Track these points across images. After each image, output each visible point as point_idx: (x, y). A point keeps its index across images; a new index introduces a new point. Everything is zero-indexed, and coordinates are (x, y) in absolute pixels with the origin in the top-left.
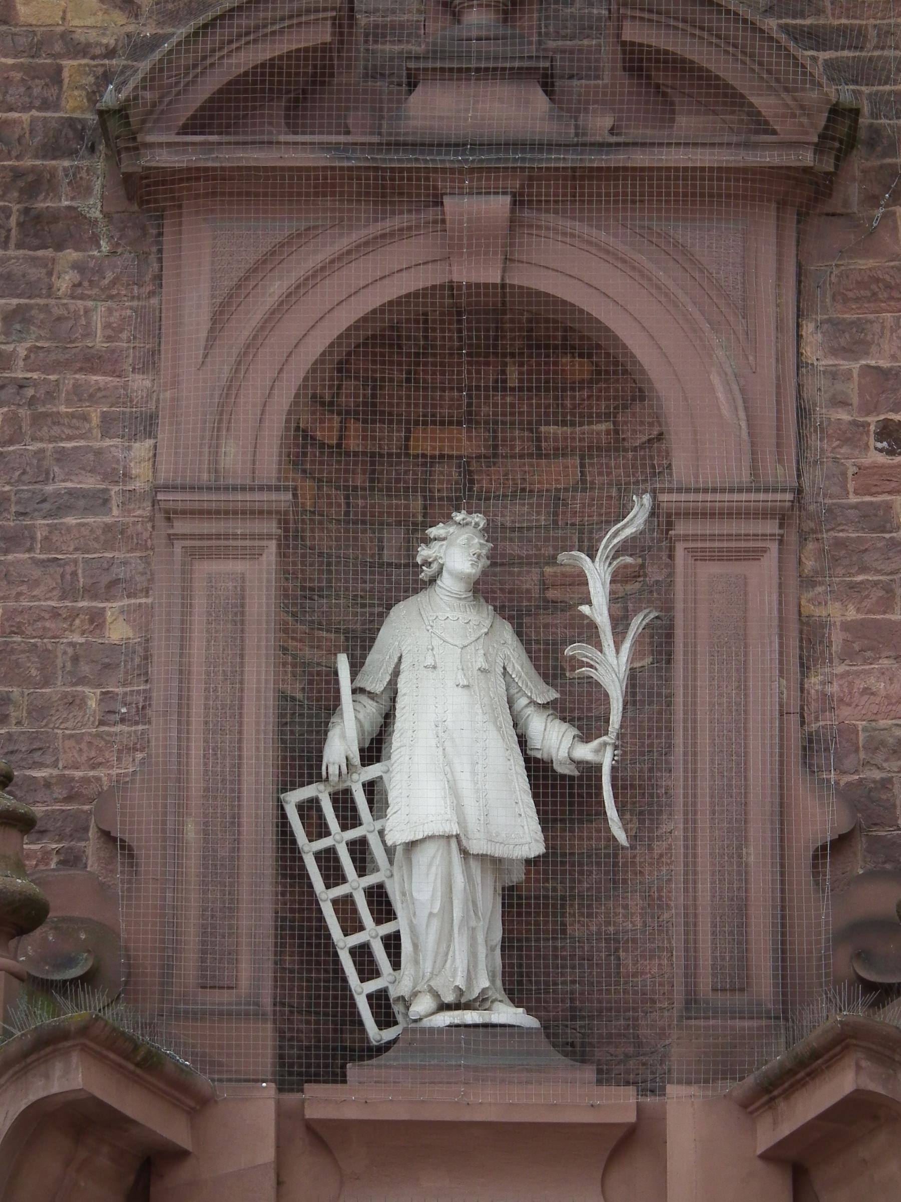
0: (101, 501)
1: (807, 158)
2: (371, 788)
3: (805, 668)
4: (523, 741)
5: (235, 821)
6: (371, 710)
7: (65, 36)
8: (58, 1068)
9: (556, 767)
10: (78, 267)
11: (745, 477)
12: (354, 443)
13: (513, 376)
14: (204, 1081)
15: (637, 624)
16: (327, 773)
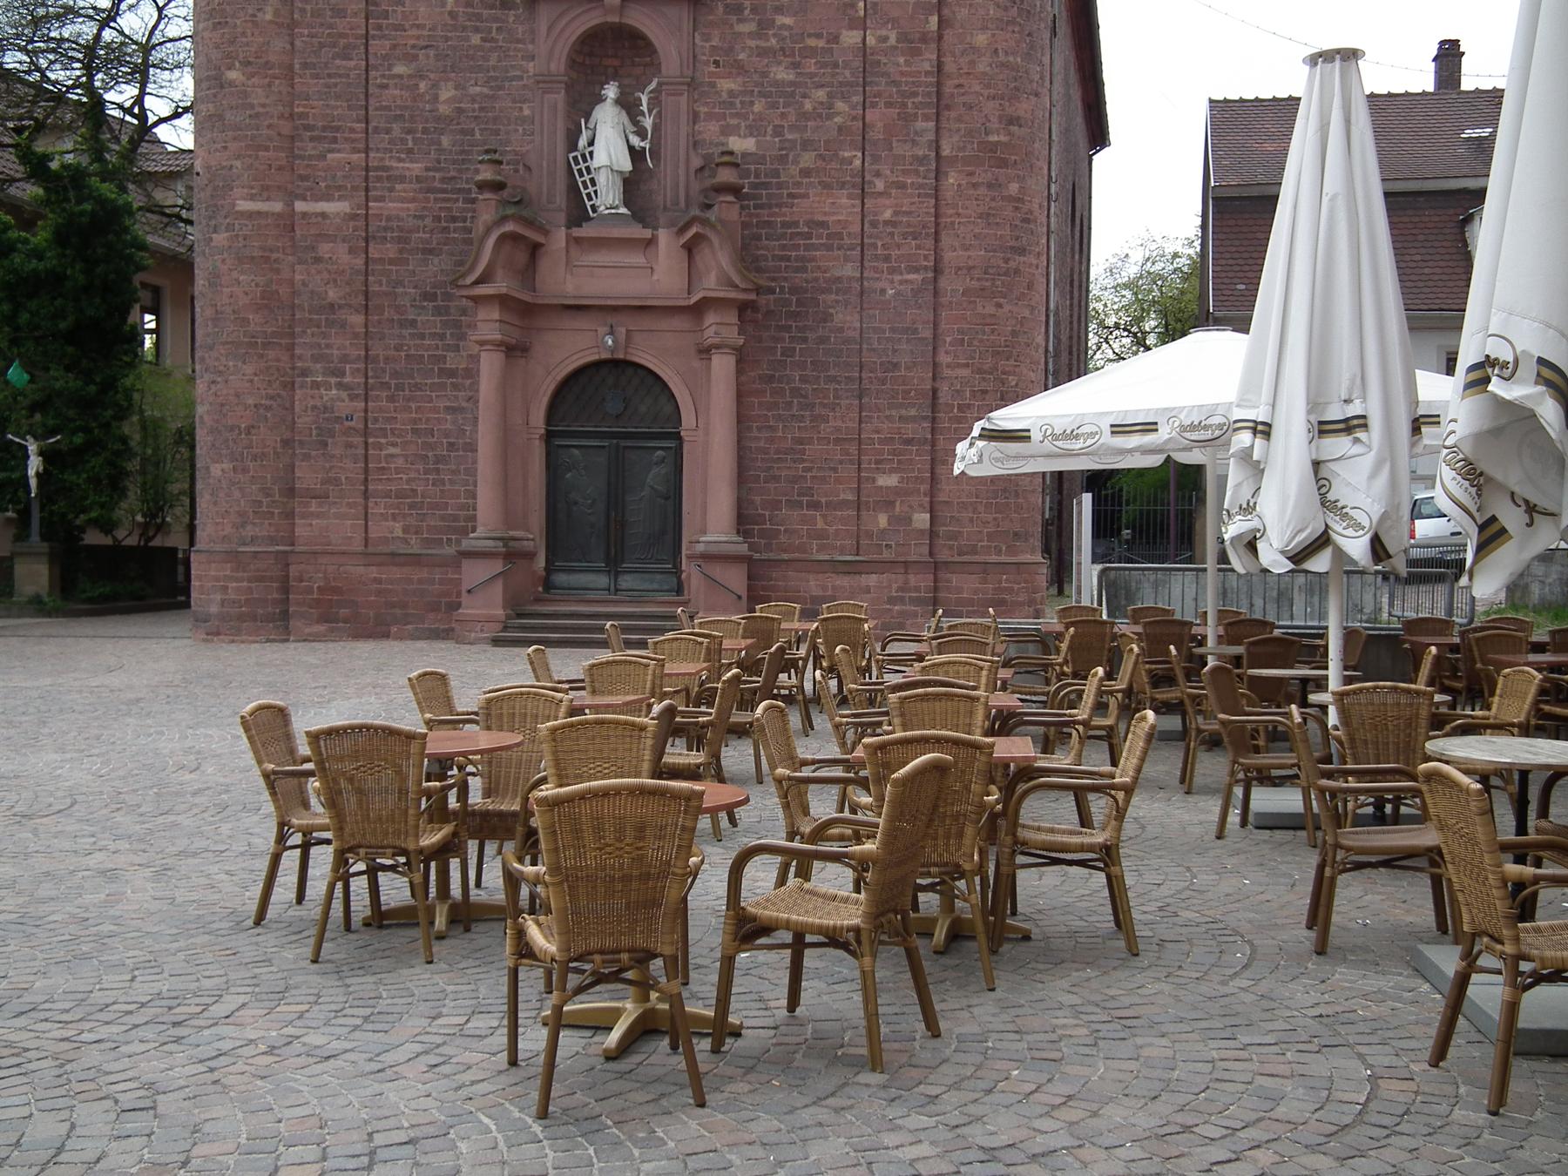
0: (521, 78)
3: (694, 123)
4: (628, 141)
6: (590, 132)
9: (130, 428)
11: (678, 73)
12: (587, 62)
13: (627, 44)
14: (547, 227)
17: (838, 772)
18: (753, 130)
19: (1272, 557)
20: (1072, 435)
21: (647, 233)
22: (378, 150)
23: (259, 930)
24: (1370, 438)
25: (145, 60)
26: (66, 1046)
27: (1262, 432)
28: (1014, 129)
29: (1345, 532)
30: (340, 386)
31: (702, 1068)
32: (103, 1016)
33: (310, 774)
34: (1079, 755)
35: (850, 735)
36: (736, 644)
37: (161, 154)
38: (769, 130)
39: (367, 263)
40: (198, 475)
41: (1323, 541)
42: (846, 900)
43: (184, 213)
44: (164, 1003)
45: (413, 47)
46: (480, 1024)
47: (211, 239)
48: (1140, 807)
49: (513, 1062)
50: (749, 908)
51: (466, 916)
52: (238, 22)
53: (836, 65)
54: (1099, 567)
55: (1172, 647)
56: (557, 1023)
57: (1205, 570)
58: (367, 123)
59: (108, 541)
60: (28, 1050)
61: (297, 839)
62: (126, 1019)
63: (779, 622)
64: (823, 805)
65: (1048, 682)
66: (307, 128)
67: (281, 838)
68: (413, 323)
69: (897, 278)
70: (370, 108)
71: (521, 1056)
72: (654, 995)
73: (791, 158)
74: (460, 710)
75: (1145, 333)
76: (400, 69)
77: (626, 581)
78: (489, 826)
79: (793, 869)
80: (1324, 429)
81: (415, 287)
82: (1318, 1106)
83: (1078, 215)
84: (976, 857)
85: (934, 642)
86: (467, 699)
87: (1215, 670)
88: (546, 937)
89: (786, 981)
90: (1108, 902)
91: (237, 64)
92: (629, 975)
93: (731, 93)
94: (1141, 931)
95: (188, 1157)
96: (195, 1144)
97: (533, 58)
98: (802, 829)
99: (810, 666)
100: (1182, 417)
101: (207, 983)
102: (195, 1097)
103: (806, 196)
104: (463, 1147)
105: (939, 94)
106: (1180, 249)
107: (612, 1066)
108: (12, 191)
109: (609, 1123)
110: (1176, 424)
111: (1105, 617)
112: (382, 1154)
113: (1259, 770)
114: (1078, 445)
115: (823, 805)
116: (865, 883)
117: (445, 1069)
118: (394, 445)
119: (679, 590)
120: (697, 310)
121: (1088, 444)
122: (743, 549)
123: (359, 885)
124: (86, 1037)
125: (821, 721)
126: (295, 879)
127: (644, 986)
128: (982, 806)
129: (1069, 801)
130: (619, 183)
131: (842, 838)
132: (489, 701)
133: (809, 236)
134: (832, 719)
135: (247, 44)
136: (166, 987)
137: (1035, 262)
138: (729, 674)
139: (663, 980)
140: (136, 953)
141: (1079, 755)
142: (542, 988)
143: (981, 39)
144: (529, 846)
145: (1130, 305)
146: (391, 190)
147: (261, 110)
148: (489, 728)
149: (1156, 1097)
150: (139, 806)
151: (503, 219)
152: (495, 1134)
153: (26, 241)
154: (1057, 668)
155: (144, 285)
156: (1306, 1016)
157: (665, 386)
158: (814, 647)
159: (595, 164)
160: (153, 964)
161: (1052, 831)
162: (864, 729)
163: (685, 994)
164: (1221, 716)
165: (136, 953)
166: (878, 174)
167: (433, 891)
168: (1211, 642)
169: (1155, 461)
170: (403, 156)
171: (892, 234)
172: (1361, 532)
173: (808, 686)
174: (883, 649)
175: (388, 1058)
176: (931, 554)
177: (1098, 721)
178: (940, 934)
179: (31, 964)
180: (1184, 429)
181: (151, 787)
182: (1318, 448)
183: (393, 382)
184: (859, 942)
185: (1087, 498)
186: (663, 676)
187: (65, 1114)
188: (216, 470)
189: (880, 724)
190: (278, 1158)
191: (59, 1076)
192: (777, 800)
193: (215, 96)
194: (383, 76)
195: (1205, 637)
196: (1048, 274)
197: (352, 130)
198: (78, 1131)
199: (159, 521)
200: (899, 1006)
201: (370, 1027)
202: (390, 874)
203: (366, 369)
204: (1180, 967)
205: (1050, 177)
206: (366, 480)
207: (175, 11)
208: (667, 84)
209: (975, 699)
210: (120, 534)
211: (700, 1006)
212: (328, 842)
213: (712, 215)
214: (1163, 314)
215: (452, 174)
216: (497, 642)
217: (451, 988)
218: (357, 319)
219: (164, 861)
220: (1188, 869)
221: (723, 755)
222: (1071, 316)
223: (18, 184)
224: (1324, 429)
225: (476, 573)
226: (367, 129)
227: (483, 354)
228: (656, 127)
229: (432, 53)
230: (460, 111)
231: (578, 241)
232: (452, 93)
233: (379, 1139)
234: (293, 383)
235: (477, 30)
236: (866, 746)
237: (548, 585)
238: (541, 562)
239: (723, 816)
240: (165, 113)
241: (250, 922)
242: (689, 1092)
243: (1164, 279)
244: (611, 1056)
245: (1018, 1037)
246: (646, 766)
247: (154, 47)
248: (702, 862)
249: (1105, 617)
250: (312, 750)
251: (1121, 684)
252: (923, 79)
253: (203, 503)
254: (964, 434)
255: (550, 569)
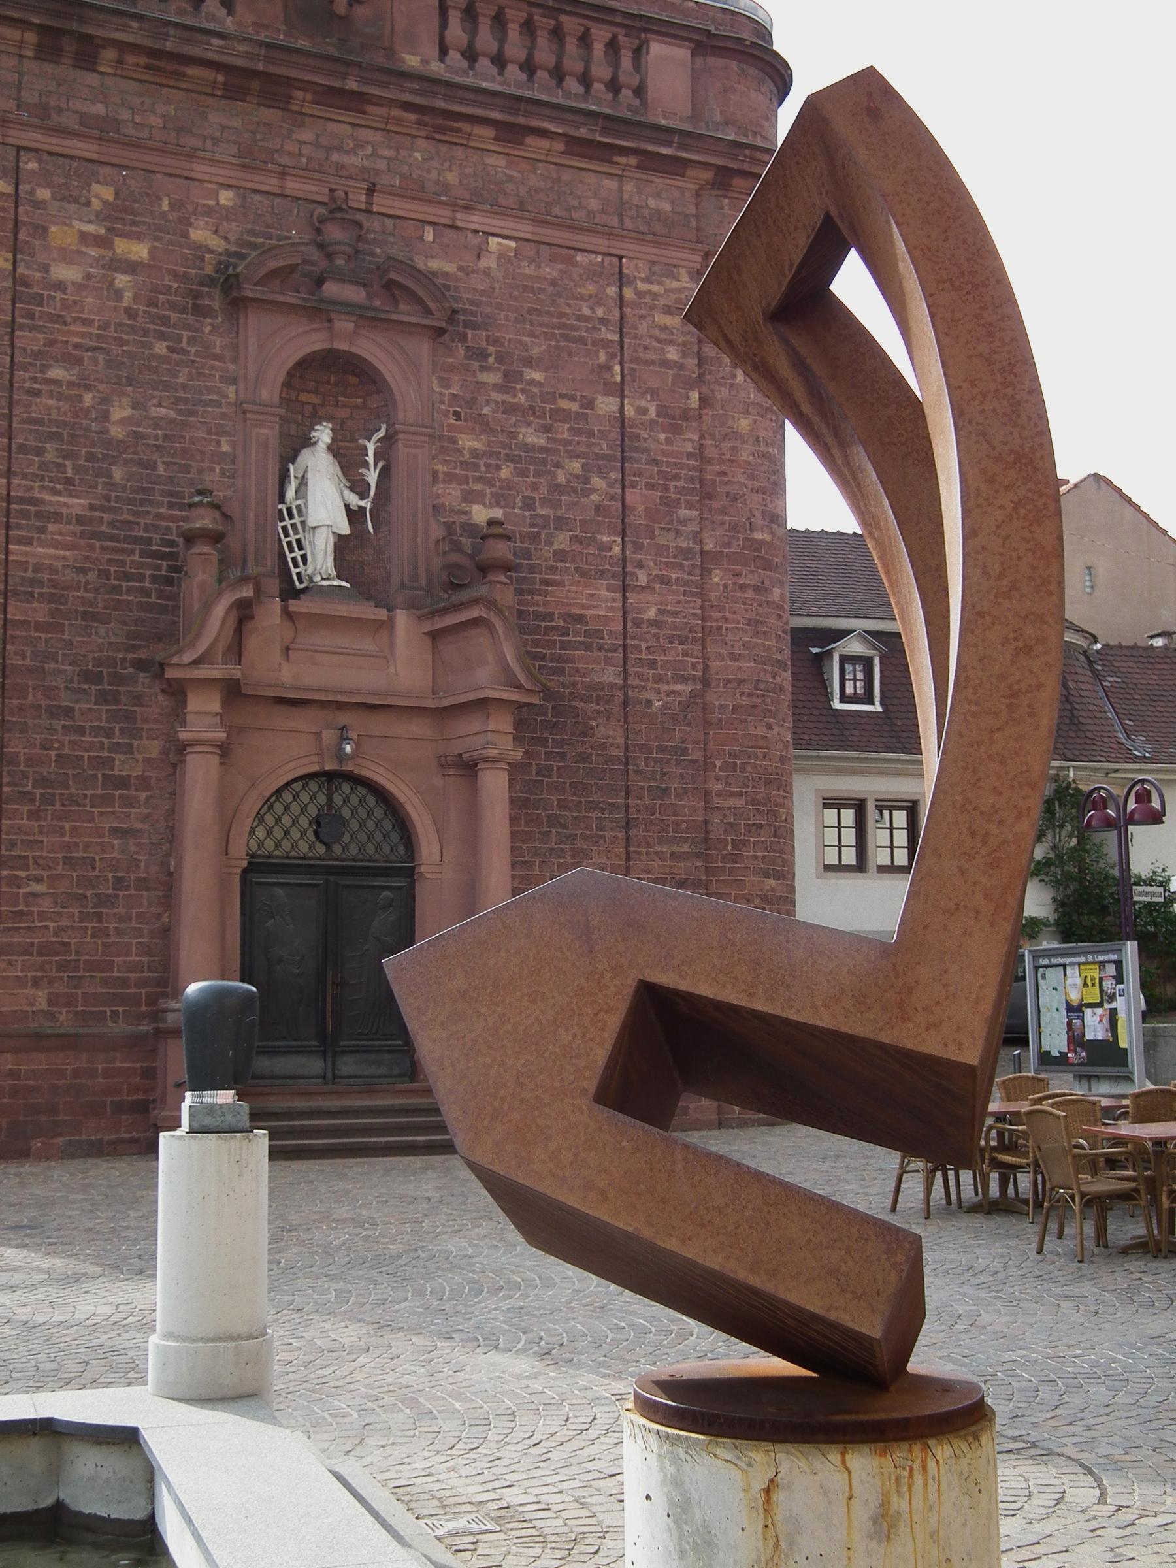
0: (218, 404)
2: (298, 507)
5: (266, 514)
7: (206, 246)
8: (245, 588)
10: (211, 325)
13: (333, 379)
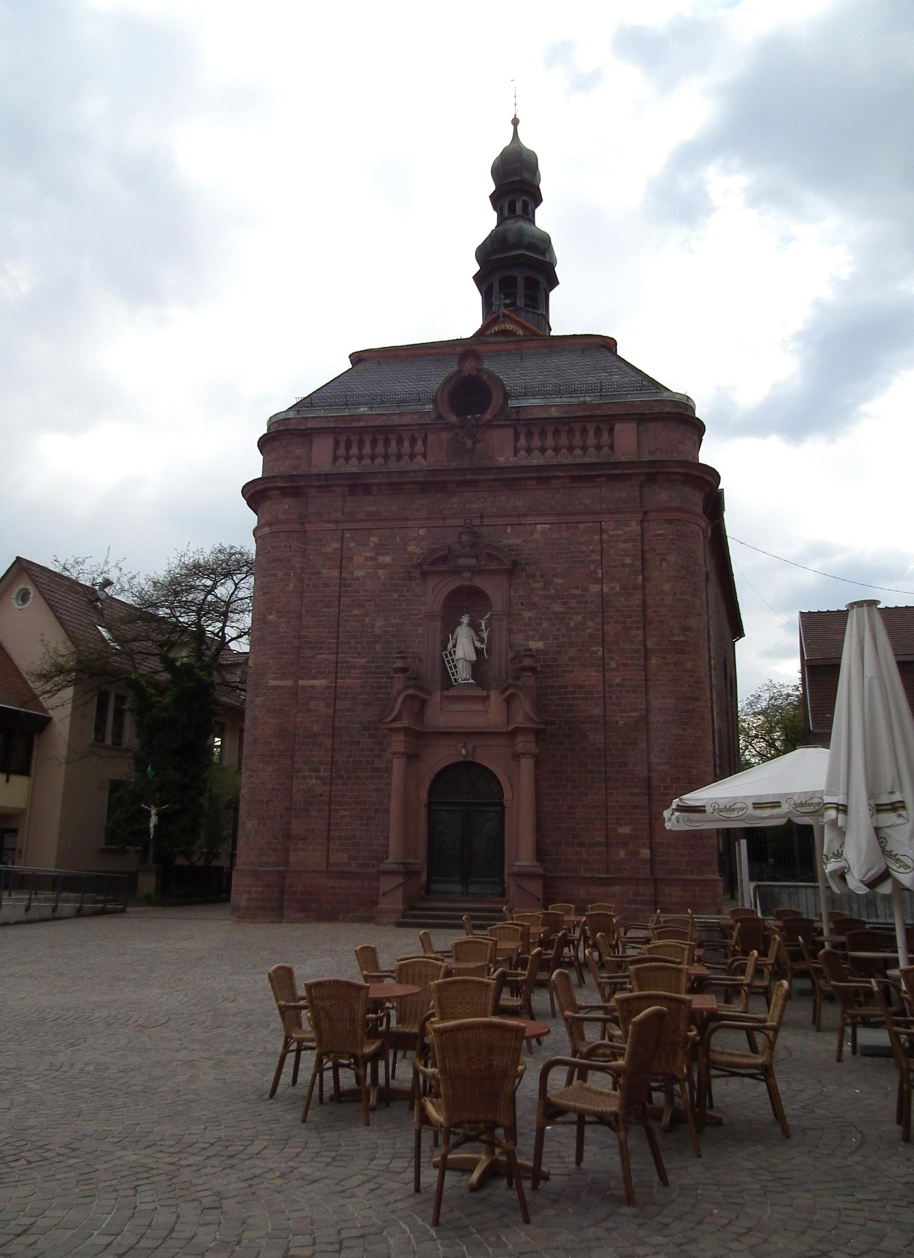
0: (418, 614)
1: (510, 567)
3: (510, 634)
4: (474, 645)
9: (204, 800)
15: (489, 629)
16: (394, 863)
17: (600, 1014)
18: (541, 638)
19: (855, 883)
20: (730, 809)
21: (485, 693)
22: (343, 653)
23: (272, 1101)
24: (908, 814)
25: (227, 609)
26: (172, 1167)
27: (842, 810)
28: (687, 633)
29: (899, 870)
30: (318, 778)
31: (527, 1198)
32: (191, 1150)
33: (305, 1007)
34: (747, 1005)
35: (607, 990)
36: (538, 930)
37: (230, 654)
38: (551, 637)
39: (334, 712)
40: (240, 827)
41: (885, 875)
42: (608, 1095)
43: (240, 686)
44: (224, 1143)
45: (363, 601)
46: (397, 1165)
47: (254, 700)
48: (785, 1039)
49: (417, 1189)
50: (552, 1098)
51: (388, 1096)
52: (275, 592)
53: (587, 603)
54: (753, 884)
55: (800, 937)
56: (444, 1166)
57: (818, 887)
58: (338, 639)
59: (188, 863)
60: (152, 1169)
61: (294, 1046)
62: (203, 1152)
63: (562, 916)
64: (592, 1034)
65: (727, 957)
66: (307, 643)
67: (286, 1045)
68: (358, 743)
69: (625, 715)
70: (340, 632)
71: (422, 1186)
72: (498, 1151)
73: (563, 652)
74: (382, 969)
75: (774, 740)
76: (355, 612)
77: (473, 889)
78: (401, 1042)
79: (576, 1073)
80: (879, 809)
81: (360, 723)
82: (907, 1243)
83: (728, 675)
84: (685, 1070)
85: (656, 932)
86: (387, 962)
87: (827, 954)
88: (437, 1112)
89: (574, 1145)
90: (769, 1101)
91: (274, 612)
92: (483, 1137)
93: (530, 618)
94: (791, 1122)
95: (240, 1238)
96: (243, 1231)
97: (424, 604)
98: (580, 1049)
99: (582, 943)
100: (795, 798)
101: (246, 1133)
102: (242, 1202)
103: (572, 671)
104: (391, 1241)
105: (645, 616)
106: (791, 692)
107: (474, 1195)
108: (157, 677)
109: (474, 1231)
110: (792, 803)
111: (759, 915)
112: (346, 1243)
113: (863, 1017)
114: (735, 814)
115: (592, 1034)
116: (619, 1085)
117: (379, 1192)
118: (345, 810)
119: (503, 894)
120: (513, 734)
121: (740, 814)
122: (540, 870)
123: (328, 1075)
124: (183, 1162)
125: (589, 978)
126: (292, 1071)
127: (492, 1145)
128: (687, 1038)
129: (743, 1035)
130: (469, 667)
131: (604, 1055)
132: (401, 966)
133: (573, 693)
134: (596, 979)
135: (279, 602)
136: (223, 1135)
137: (704, 705)
138: (535, 951)
139: (504, 1141)
140: (207, 1112)
141: (747, 1005)
142: (432, 1144)
143: (667, 587)
144: (425, 1053)
145: (764, 723)
146: (349, 673)
147: (284, 634)
148: (400, 982)
149: (804, 1232)
150: (204, 1022)
151: (407, 688)
152: (409, 1234)
153: (160, 702)
154: (731, 948)
155: (217, 723)
156: (898, 1182)
157: (494, 776)
158: (583, 932)
159: (457, 657)
160: (215, 1120)
161: (731, 1054)
162: (616, 987)
163: (516, 1151)
164: (833, 983)
165: (207, 1112)
166: (612, 659)
167: (368, 1080)
168: (826, 933)
169: (781, 822)
170: (356, 655)
171: (621, 691)
172: (908, 870)
173: (581, 955)
174: (625, 934)
175: (348, 1184)
176: (652, 874)
177: (758, 983)
178: (666, 1118)
179: (152, 1117)
180: (796, 805)
181: (210, 1011)
182: (877, 820)
183: (346, 775)
184: (617, 1121)
185: (743, 842)
186: (496, 950)
187: (174, 1209)
188: (249, 825)
189: (625, 983)
190: (289, 1241)
191: (170, 1185)
192: (564, 1029)
193: (261, 628)
194: (347, 616)
195: (822, 929)
196: (712, 710)
197: (330, 643)
198: (181, 1219)
199: (215, 851)
200: (642, 1162)
201: (335, 1163)
202: (346, 1069)
203: (332, 768)
204: (817, 1147)
205: (710, 657)
206: (329, 830)
207: (242, 585)
208: (495, 615)
209: (680, 970)
210: (195, 859)
211: (525, 1160)
212: (312, 1048)
213: (520, 683)
214: (785, 729)
215: (381, 664)
216: (399, 925)
217: (380, 1142)
218: (328, 741)
219: (219, 1057)
220: (820, 1082)
221: (532, 998)
222: (728, 732)
223: (161, 674)
224: (879, 809)
225: (387, 883)
226: (338, 642)
227: (395, 760)
228: (489, 637)
229: (372, 603)
230: (386, 632)
231: (447, 698)
232: (382, 623)
233: (345, 1234)
234: (292, 776)
235: (396, 591)
236: (617, 1000)
237: (428, 891)
238: (424, 877)
239: (534, 1042)
240: (234, 636)
241: (267, 1096)
242: (520, 1214)
243: (783, 709)
244: (475, 1188)
245: (715, 1188)
246: (490, 1009)
247: (232, 603)
248: (525, 1068)
249: (759, 915)
250: (307, 993)
251: (770, 960)
252: (635, 608)
253: (241, 843)
254: (668, 807)
255: (429, 881)
